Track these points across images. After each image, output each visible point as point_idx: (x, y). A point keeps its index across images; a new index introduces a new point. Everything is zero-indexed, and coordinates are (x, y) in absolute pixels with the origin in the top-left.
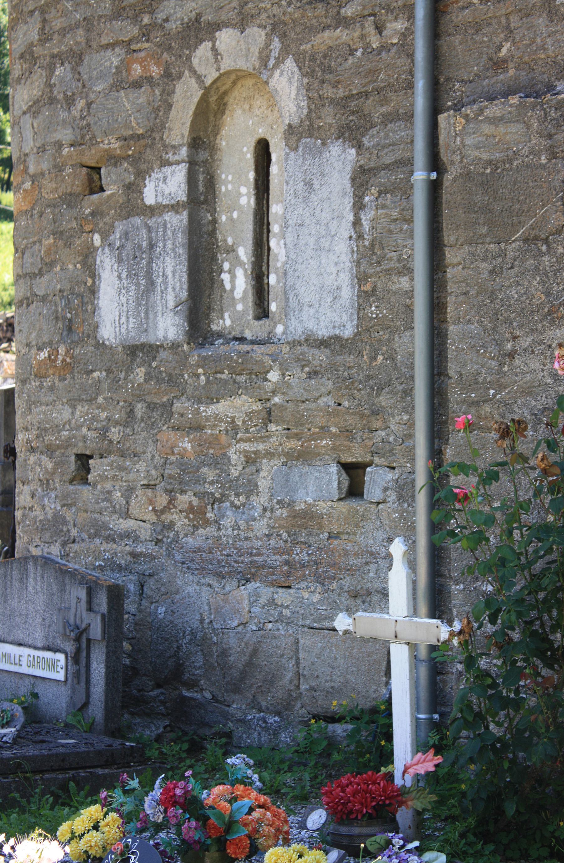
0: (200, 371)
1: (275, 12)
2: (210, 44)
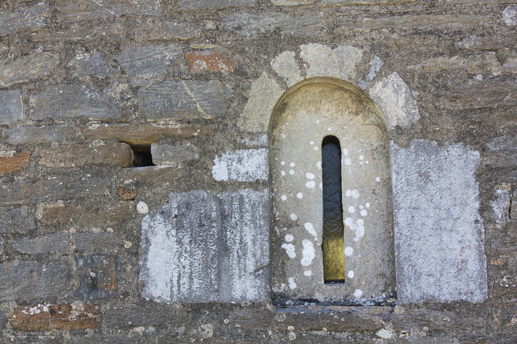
0: (290, 328)
1: (374, 37)
2: (293, 53)
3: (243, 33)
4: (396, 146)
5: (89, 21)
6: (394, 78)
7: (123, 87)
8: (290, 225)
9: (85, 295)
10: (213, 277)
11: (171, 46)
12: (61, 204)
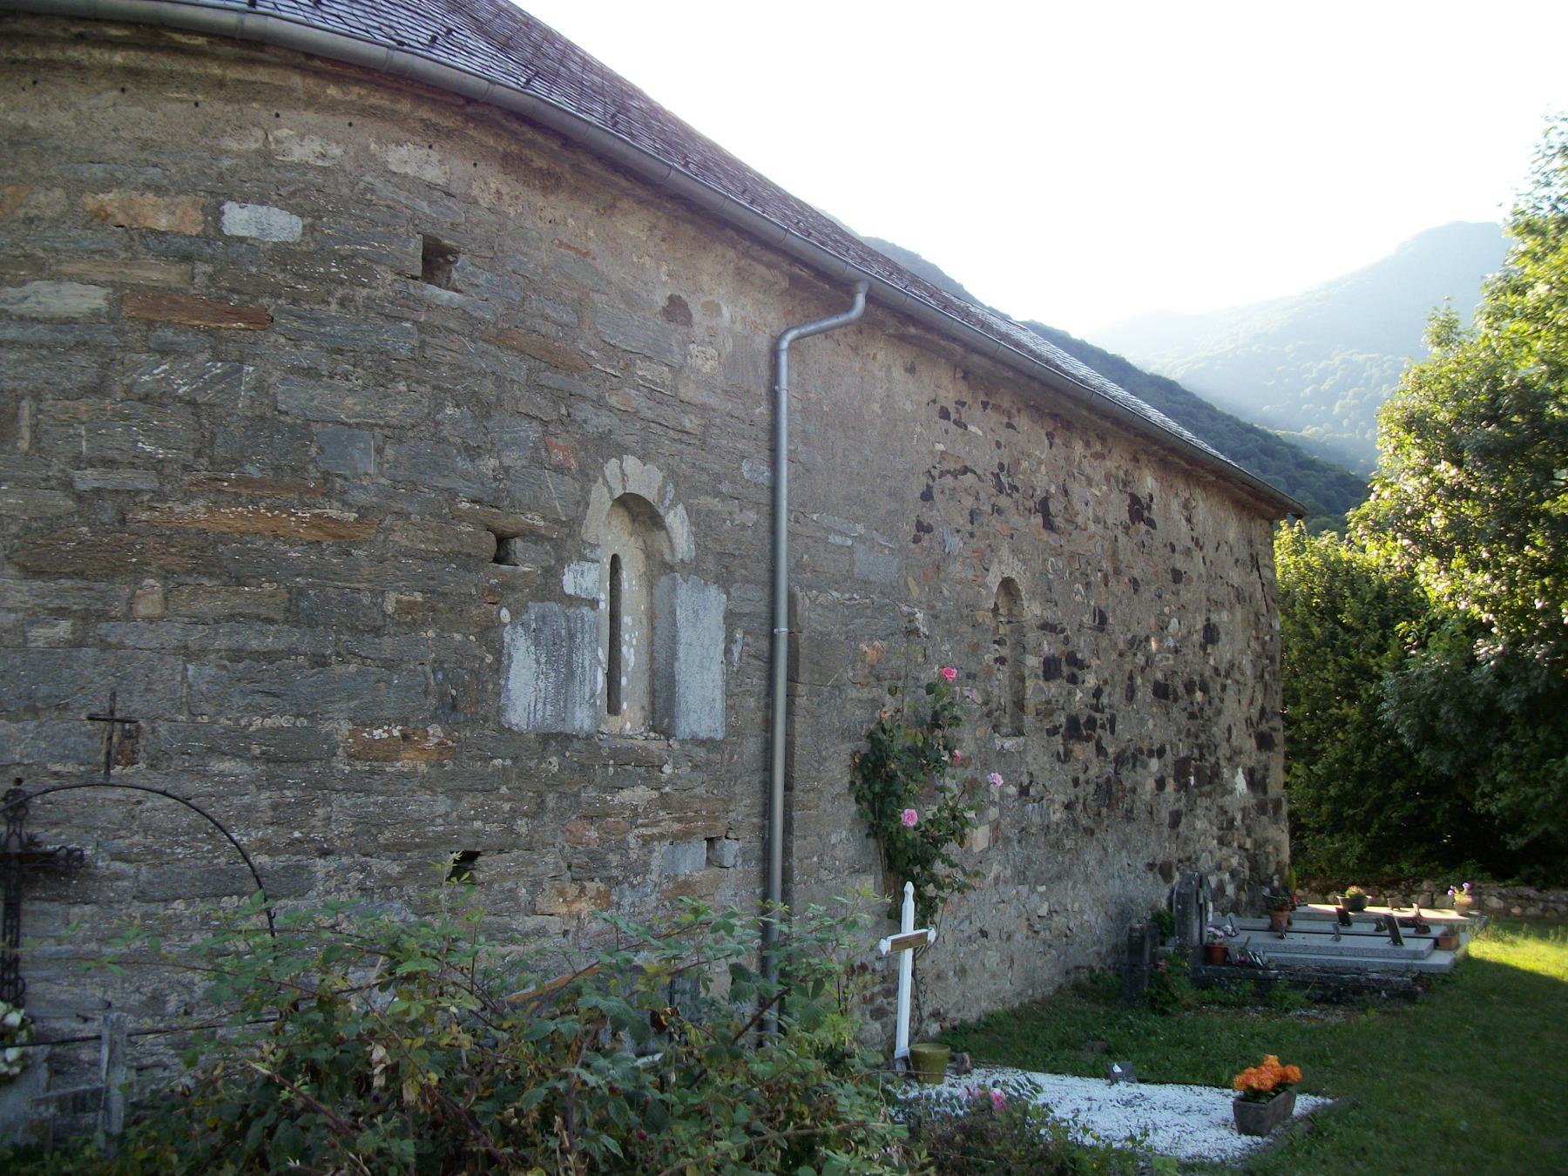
11: (534, 424)
12: (419, 597)
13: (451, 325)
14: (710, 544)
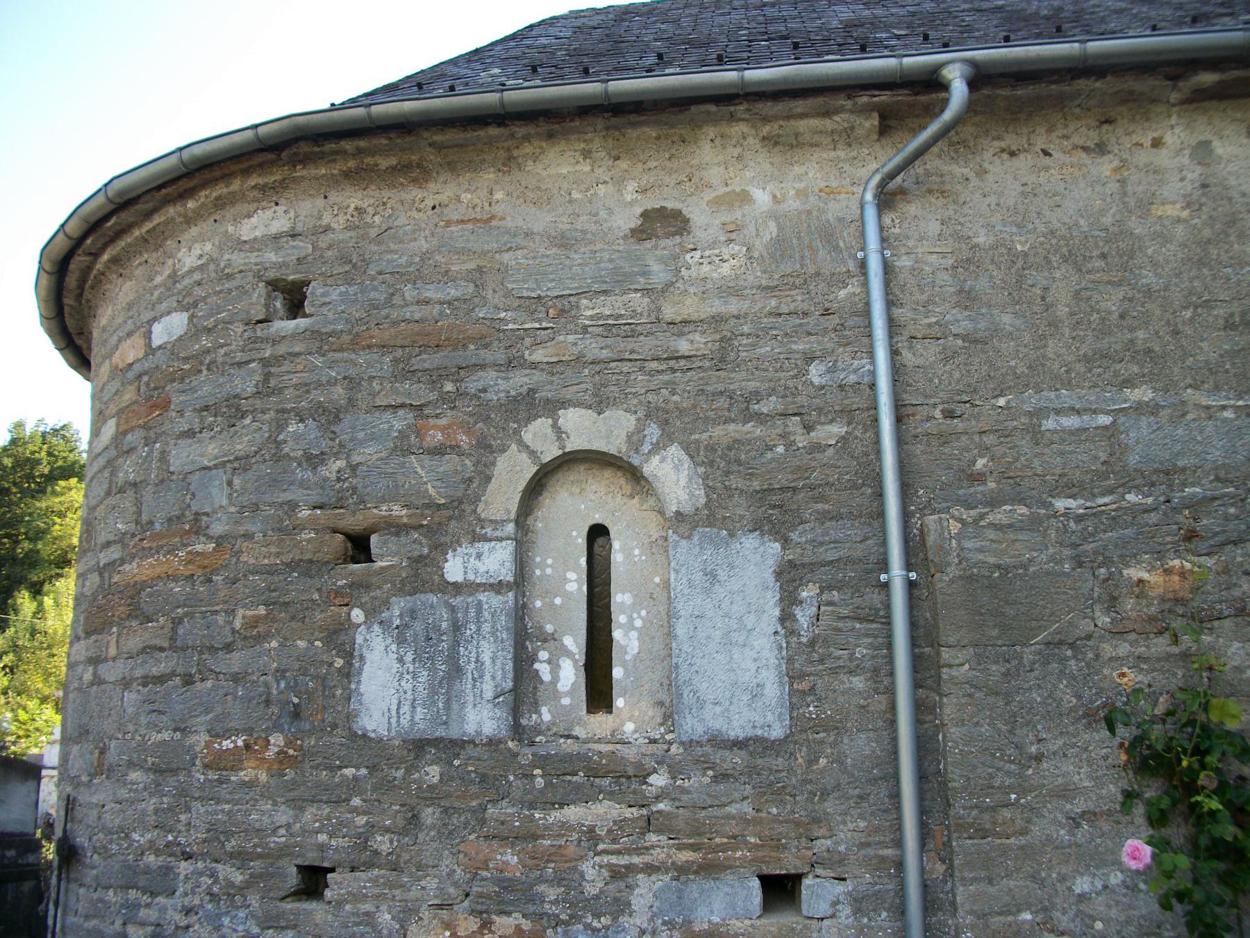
0: (537, 772)
2: (550, 421)
3: (488, 396)
4: (676, 537)
5: (306, 385)
6: (674, 451)
7: (340, 464)
8: (546, 639)
9: (286, 727)
10: (441, 705)
11: (401, 412)
12: (262, 610)
13: (297, 349)
14: (735, 482)
